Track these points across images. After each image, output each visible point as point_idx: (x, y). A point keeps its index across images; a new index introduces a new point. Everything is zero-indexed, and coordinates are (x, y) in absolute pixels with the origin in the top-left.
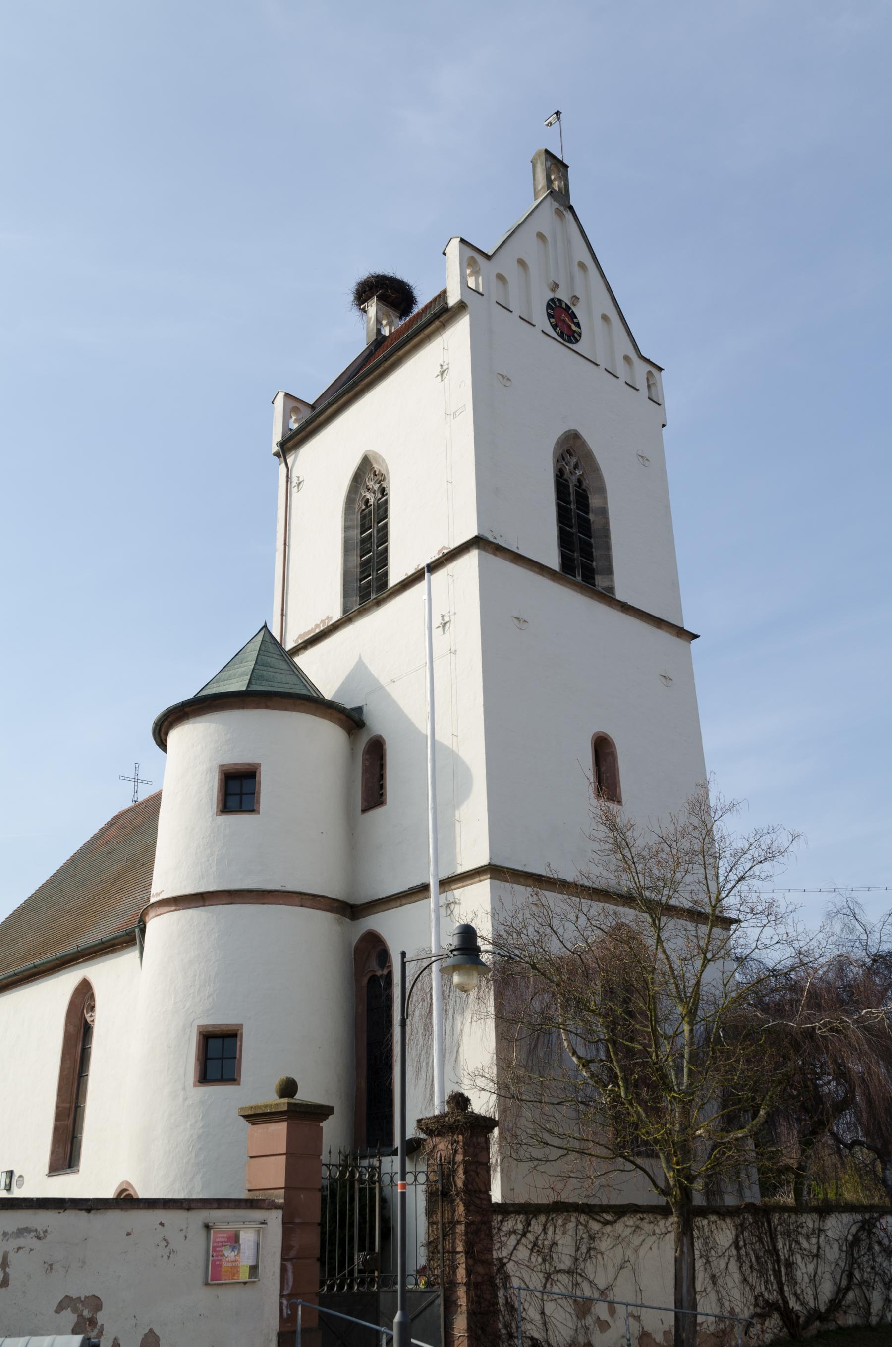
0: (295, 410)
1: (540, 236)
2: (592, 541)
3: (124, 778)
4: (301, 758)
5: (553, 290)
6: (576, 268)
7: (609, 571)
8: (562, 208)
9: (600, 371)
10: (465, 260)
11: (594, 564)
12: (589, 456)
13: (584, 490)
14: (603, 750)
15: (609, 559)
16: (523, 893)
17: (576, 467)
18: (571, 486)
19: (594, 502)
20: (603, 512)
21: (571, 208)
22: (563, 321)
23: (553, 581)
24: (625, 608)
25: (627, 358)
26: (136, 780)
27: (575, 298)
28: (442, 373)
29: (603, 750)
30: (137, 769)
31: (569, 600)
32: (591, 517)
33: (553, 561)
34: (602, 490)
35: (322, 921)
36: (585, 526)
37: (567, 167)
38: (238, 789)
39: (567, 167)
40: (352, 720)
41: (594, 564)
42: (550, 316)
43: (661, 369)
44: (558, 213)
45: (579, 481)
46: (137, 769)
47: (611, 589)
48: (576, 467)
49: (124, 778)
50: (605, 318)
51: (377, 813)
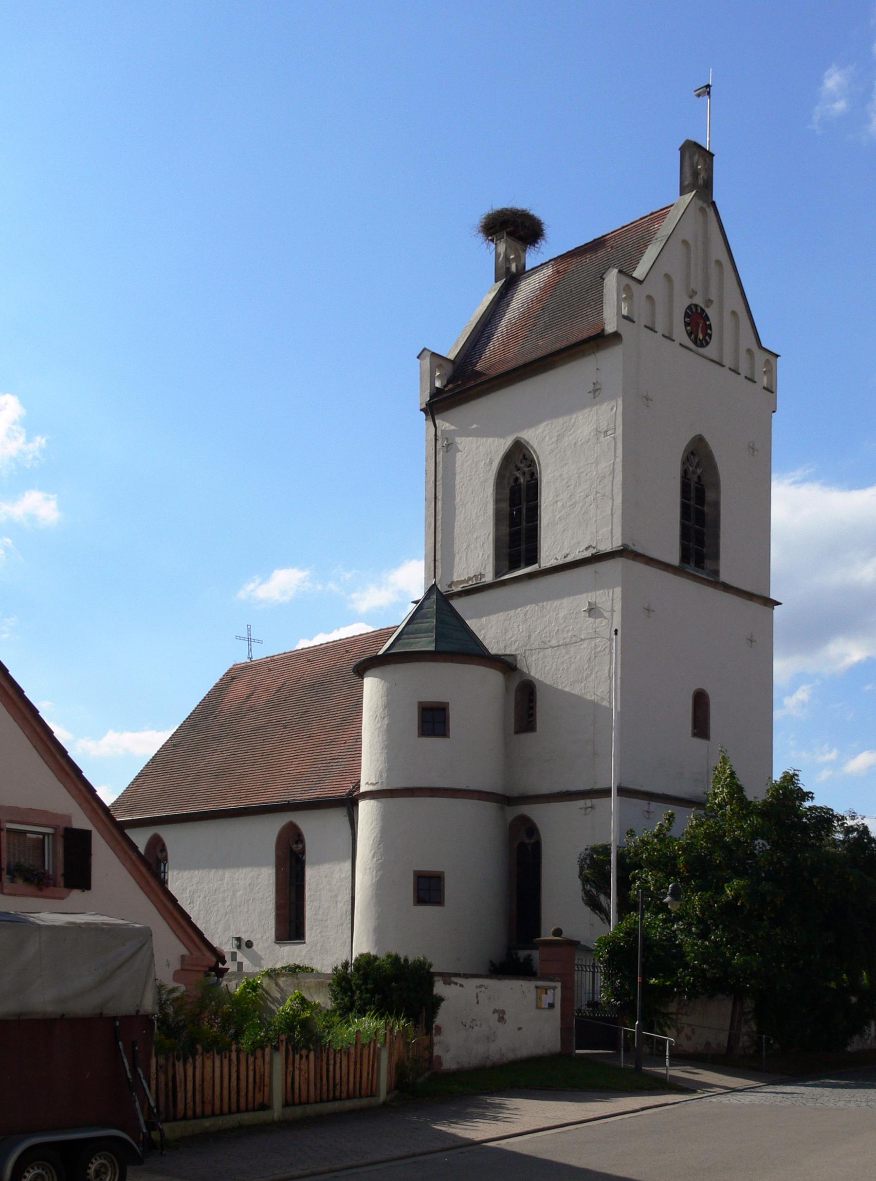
0: (440, 366)
1: (685, 242)
2: (705, 530)
3: (240, 638)
4: (472, 695)
5: (691, 297)
6: (713, 264)
7: (716, 556)
8: (705, 206)
9: (725, 370)
10: (622, 288)
11: (705, 550)
12: (710, 456)
13: (702, 485)
14: (700, 700)
15: (717, 546)
16: (641, 804)
17: (698, 465)
18: (692, 484)
19: (709, 496)
20: (716, 505)
21: (714, 203)
22: (698, 324)
23: (675, 574)
24: (727, 588)
25: (749, 351)
26: (249, 640)
27: (709, 302)
28: (595, 391)
29: (700, 700)
30: (249, 630)
31: (686, 589)
32: (706, 509)
33: (674, 557)
34: (716, 486)
35: (489, 808)
36: (700, 517)
37: (713, 155)
38: (433, 720)
39: (713, 155)
40: (506, 665)
41: (705, 550)
42: (687, 324)
43: (777, 356)
44: (702, 210)
45: (699, 477)
46: (249, 630)
47: (716, 573)
48: (698, 465)
49: (240, 638)
50: (734, 313)
51: (527, 738)
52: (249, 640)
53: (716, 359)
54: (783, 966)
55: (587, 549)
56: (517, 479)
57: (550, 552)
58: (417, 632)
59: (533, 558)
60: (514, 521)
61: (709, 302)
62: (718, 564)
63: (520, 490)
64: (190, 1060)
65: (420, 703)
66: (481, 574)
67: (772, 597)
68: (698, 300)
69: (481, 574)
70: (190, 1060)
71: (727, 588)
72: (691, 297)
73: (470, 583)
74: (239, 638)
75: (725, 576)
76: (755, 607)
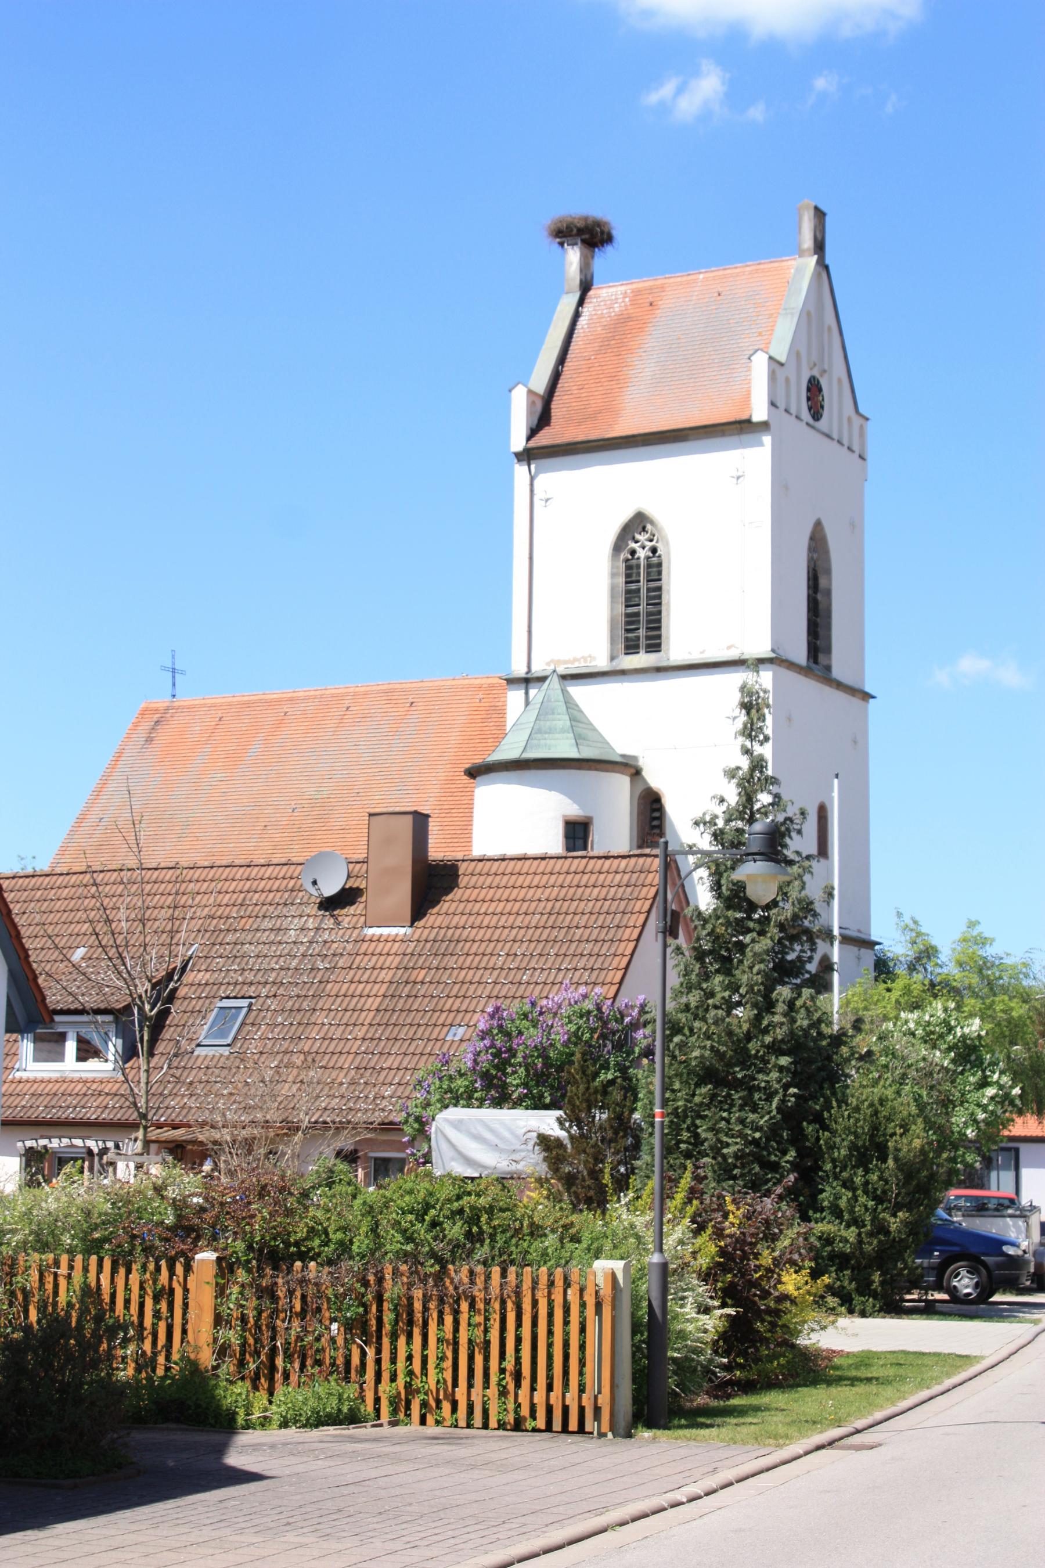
2: (818, 620)
24: (839, 685)
26: (174, 671)
30: (173, 657)
46: (173, 657)
47: (828, 668)
52: (174, 671)
53: (826, 431)
54: (72, 1341)
55: (729, 648)
56: (633, 552)
57: (679, 644)
58: (550, 731)
59: (655, 645)
60: (631, 597)
61: (823, 372)
62: (830, 659)
63: (638, 566)
64: (122, 1271)
65: (564, 816)
66: (590, 656)
67: (868, 689)
68: (816, 373)
69: (590, 656)
70: (122, 1271)
71: (839, 685)
72: (811, 369)
73: (577, 664)
74: (183, 673)
75: (837, 673)
76: (856, 702)
